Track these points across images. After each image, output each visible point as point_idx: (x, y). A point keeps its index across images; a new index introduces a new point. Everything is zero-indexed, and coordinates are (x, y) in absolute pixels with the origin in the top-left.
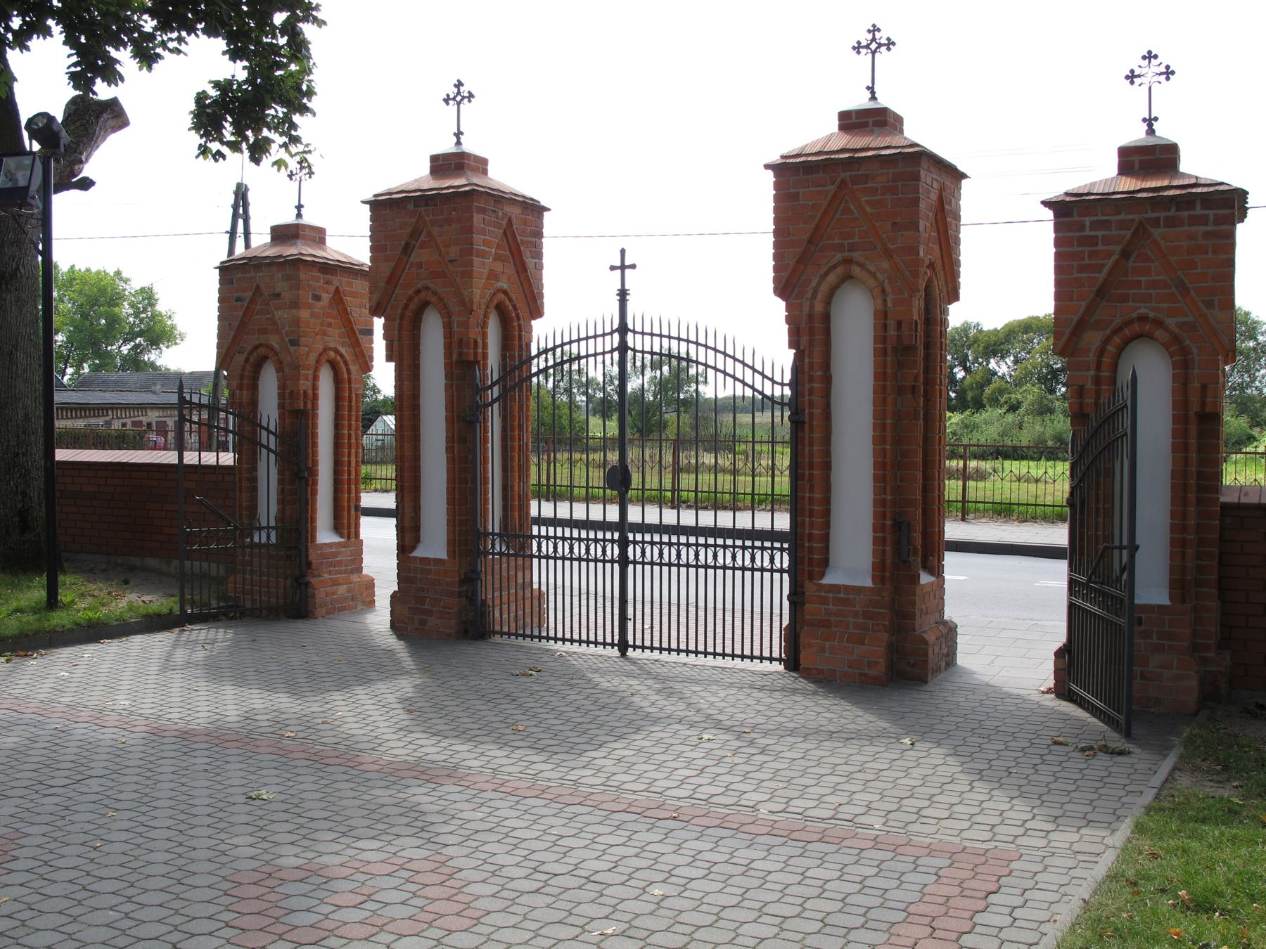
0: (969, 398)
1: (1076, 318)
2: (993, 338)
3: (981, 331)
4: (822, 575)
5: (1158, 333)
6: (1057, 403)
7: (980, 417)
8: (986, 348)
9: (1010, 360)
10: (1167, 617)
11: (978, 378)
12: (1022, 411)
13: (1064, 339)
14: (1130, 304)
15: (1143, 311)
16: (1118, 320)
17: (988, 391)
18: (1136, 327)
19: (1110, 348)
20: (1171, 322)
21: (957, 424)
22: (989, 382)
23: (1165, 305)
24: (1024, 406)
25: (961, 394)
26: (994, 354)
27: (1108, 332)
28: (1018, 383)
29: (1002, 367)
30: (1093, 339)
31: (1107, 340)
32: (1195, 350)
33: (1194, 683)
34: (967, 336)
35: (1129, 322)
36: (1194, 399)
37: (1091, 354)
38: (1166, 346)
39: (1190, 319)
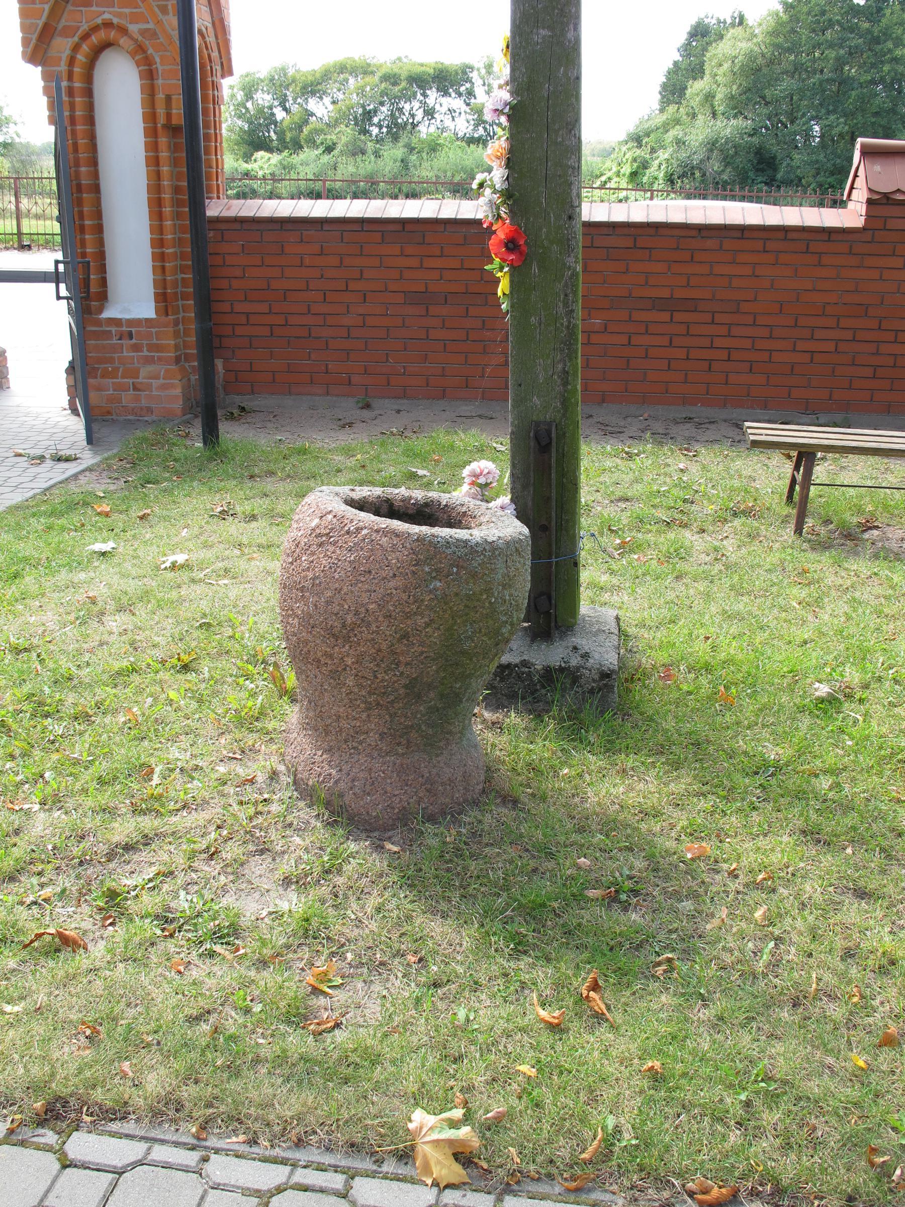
0: (288, 140)
1: (41, 23)
2: (310, 78)
3: (298, 71)
4: (101, 310)
5: (123, 41)
6: (369, 144)
7: (296, 159)
8: (304, 87)
9: (327, 100)
10: (153, 330)
11: (296, 119)
12: (336, 152)
13: (32, 46)
14: (94, 8)
15: (106, 16)
16: (85, 27)
17: (306, 130)
18: (102, 34)
19: (80, 57)
20: (133, 28)
21: (276, 166)
22: (306, 122)
23: (127, 11)
24: (339, 147)
25: (281, 135)
26: (313, 93)
27: (76, 39)
28: (333, 124)
29: (321, 108)
30: (62, 46)
31: (76, 48)
32: (158, 60)
33: (178, 391)
34: (285, 75)
35: (95, 29)
36: (161, 111)
37: (63, 63)
38: (133, 54)
39: (151, 26)
